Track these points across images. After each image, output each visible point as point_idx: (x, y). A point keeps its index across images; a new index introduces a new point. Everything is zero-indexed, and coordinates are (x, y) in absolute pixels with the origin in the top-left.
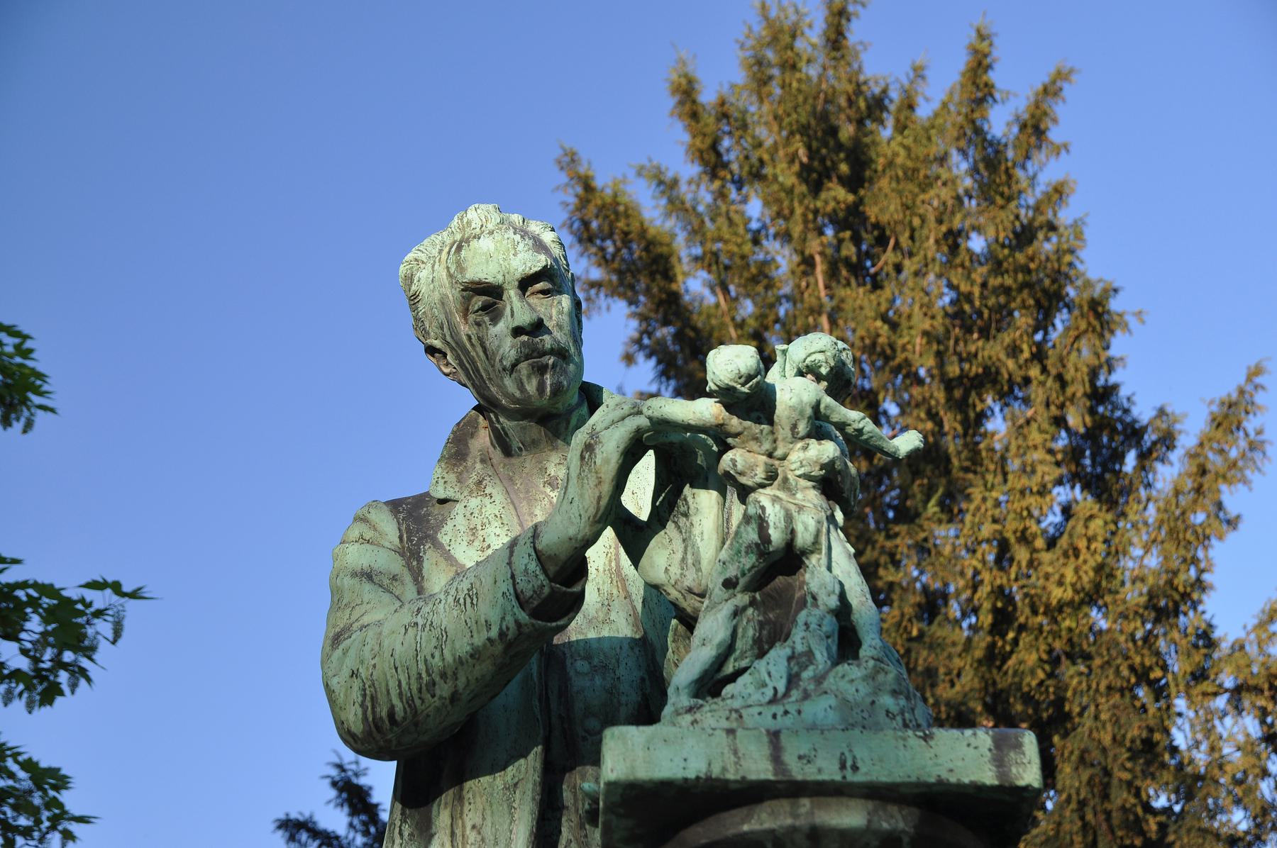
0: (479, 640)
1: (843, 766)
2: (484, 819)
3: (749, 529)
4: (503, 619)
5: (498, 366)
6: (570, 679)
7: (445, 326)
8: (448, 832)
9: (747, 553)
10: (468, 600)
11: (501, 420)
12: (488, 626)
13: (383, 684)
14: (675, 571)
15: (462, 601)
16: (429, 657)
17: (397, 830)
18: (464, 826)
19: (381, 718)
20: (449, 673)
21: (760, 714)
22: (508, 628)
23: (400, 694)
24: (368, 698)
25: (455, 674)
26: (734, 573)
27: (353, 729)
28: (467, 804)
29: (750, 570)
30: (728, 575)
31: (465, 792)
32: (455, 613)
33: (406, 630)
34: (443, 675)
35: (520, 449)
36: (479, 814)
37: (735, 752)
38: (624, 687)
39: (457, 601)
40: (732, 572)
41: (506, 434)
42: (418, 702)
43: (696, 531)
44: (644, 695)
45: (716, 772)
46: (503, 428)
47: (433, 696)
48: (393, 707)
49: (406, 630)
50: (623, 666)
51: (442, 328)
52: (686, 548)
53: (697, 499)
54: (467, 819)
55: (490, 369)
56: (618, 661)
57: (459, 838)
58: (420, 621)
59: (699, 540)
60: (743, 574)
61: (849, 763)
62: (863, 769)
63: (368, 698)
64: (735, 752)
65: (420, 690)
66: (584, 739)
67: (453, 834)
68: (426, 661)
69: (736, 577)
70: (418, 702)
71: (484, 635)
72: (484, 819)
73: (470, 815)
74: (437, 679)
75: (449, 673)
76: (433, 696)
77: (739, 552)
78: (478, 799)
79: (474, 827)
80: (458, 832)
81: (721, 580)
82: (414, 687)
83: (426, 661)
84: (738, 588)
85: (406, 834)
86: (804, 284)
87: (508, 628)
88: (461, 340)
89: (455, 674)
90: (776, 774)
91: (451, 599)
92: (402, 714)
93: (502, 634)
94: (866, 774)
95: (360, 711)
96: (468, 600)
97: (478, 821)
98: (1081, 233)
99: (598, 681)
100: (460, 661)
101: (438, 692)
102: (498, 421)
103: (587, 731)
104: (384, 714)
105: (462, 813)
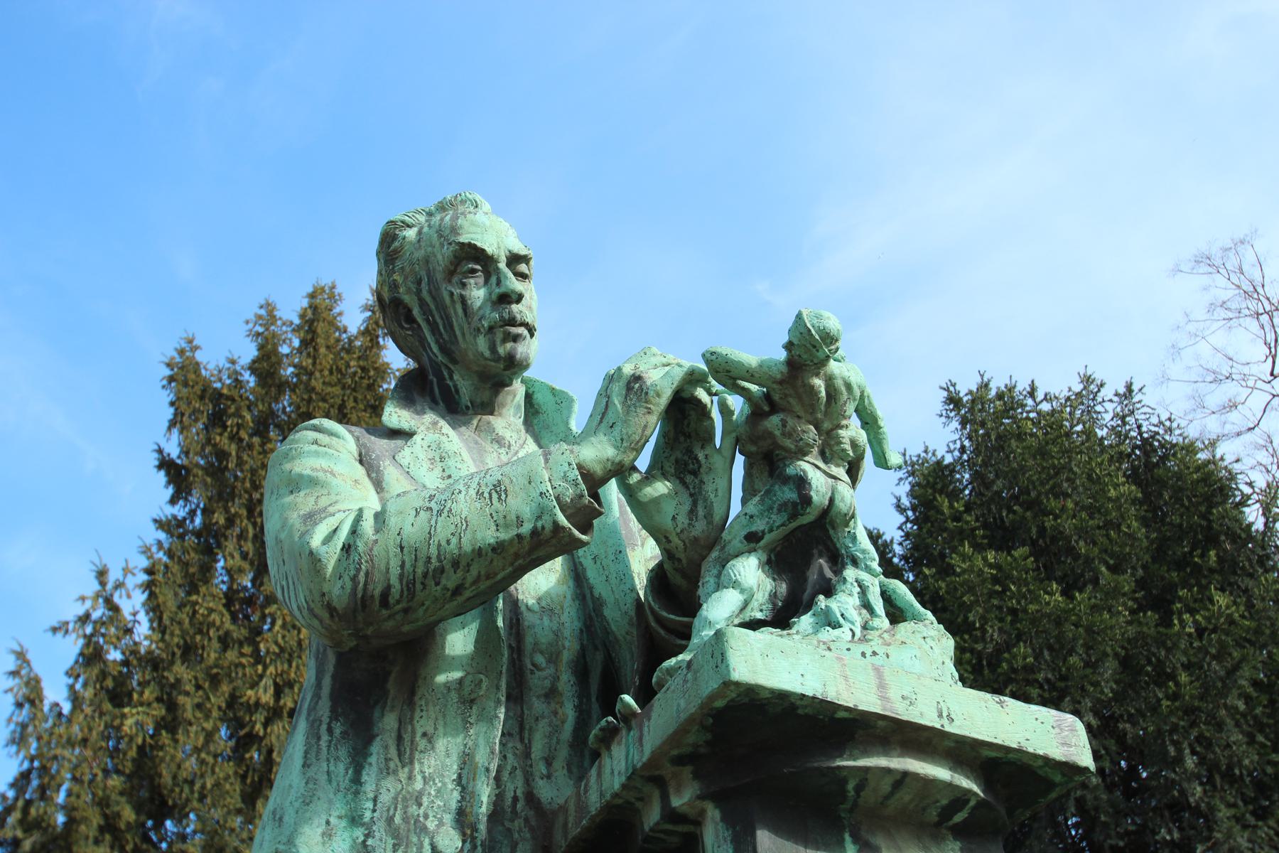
0: (504, 535)
1: (940, 716)
2: (436, 729)
3: (786, 489)
4: (539, 518)
5: (475, 323)
6: (521, 613)
7: (424, 285)
8: (394, 735)
9: (779, 511)
10: (495, 496)
11: (455, 377)
12: (520, 522)
13: (384, 562)
14: (683, 520)
15: (486, 495)
16: (444, 543)
17: (324, 727)
18: (413, 732)
19: (372, 596)
20: (463, 563)
21: (848, 649)
22: (543, 528)
23: (401, 577)
24: (362, 574)
25: (469, 565)
26: (761, 528)
27: (335, 603)
28: (418, 711)
29: (778, 527)
30: (754, 529)
31: (416, 698)
32: (478, 506)
33: (417, 513)
34: (456, 564)
35: (467, 408)
36: (431, 723)
37: (846, 678)
38: (567, 633)
39: (480, 494)
40: (759, 526)
41: (457, 391)
42: (419, 587)
43: (709, 488)
44: (582, 644)
46: (455, 386)
47: (437, 584)
48: (389, 587)
49: (417, 513)
50: (566, 614)
51: (419, 282)
52: (695, 504)
53: (711, 460)
54: (417, 726)
55: (466, 326)
56: (562, 608)
57: (407, 743)
58: (433, 505)
59: (712, 496)
60: (771, 531)
61: (945, 714)
62: (956, 722)
63: (362, 574)
64: (846, 678)
65: (425, 575)
66: (532, 672)
67: (400, 739)
68: (439, 545)
69: (763, 531)
70: (419, 587)
71: (513, 532)
72: (436, 729)
73: (422, 722)
74: (448, 566)
75: (463, 563)
76: (437, 584)
77: (772, 508)
78: (431, 708)
79: (424, 735)
80: (407, 737)
81: (744, 533)
82: (420, 571)
83: (439, 545)
84: (762, 543)
85: (337, 731)
86: (219, 518)
87: (543, 528)
88: (443, 300)
89: (469, 565)
90: (885, 709)
91: (472, 492)
92: (397, 596)
93: (535, 532)
94: (959, 727)
95: (349, 585)
96: (495, 496)
97: (430, 730)
98: (18, 659)
99: (546, 621)
100: (479, 552)
101: (444, 581)
102: (451, 378)
103: (534, 665)
104: (377, 592)
105: (412, 719)
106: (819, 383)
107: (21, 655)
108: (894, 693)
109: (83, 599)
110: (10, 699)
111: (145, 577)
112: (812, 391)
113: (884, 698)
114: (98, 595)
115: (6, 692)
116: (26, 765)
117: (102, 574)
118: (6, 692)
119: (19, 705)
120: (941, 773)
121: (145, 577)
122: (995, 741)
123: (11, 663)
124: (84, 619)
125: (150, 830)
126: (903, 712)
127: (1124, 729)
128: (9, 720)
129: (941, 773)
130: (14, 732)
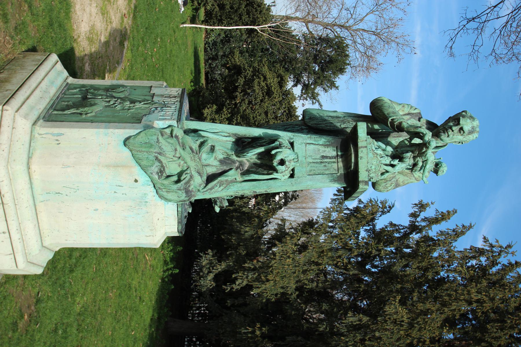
45: (359, 138)
106: (424, 149)
107: (470, 227)
108: (362, 149)
109: (497, 241)
110: (455, 227)
111: (514, 262)
112: (422, 149)
113: (362, 147)
114: (501, 247)
115: (456, 225)
116: (435, 238)
117: (509, 246)
118: (456, 225)
119: (454, 231)
120: (353, 160)
121: (514, 262)
122: (78, 129)
123: (467, 224)
124: (492, 246)
125: (456, 320)
126: (360, 151)
127: (236, 97)
128: (448, 229)
129: (353, 160)
130: (445, 231)
